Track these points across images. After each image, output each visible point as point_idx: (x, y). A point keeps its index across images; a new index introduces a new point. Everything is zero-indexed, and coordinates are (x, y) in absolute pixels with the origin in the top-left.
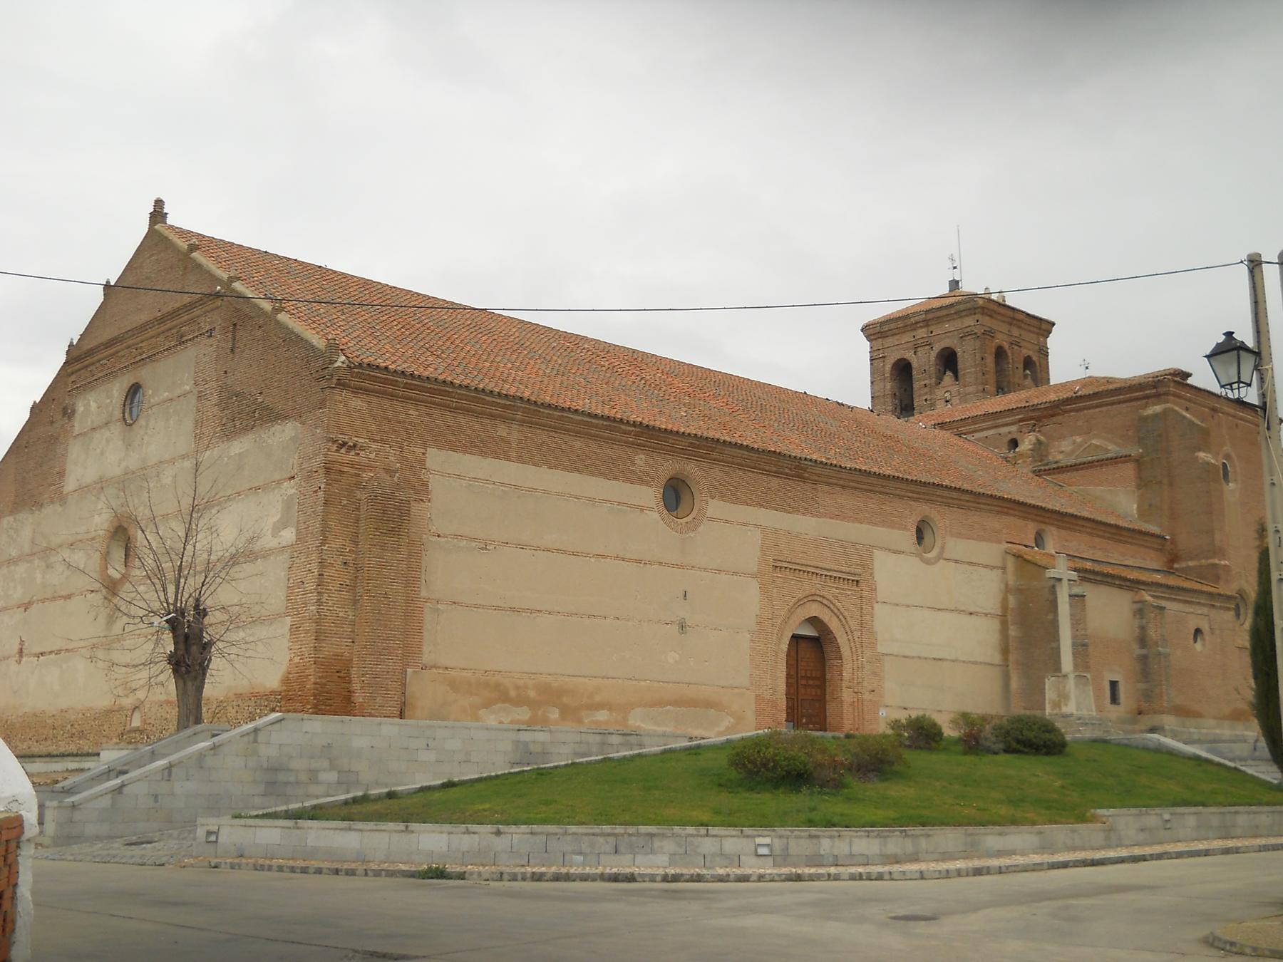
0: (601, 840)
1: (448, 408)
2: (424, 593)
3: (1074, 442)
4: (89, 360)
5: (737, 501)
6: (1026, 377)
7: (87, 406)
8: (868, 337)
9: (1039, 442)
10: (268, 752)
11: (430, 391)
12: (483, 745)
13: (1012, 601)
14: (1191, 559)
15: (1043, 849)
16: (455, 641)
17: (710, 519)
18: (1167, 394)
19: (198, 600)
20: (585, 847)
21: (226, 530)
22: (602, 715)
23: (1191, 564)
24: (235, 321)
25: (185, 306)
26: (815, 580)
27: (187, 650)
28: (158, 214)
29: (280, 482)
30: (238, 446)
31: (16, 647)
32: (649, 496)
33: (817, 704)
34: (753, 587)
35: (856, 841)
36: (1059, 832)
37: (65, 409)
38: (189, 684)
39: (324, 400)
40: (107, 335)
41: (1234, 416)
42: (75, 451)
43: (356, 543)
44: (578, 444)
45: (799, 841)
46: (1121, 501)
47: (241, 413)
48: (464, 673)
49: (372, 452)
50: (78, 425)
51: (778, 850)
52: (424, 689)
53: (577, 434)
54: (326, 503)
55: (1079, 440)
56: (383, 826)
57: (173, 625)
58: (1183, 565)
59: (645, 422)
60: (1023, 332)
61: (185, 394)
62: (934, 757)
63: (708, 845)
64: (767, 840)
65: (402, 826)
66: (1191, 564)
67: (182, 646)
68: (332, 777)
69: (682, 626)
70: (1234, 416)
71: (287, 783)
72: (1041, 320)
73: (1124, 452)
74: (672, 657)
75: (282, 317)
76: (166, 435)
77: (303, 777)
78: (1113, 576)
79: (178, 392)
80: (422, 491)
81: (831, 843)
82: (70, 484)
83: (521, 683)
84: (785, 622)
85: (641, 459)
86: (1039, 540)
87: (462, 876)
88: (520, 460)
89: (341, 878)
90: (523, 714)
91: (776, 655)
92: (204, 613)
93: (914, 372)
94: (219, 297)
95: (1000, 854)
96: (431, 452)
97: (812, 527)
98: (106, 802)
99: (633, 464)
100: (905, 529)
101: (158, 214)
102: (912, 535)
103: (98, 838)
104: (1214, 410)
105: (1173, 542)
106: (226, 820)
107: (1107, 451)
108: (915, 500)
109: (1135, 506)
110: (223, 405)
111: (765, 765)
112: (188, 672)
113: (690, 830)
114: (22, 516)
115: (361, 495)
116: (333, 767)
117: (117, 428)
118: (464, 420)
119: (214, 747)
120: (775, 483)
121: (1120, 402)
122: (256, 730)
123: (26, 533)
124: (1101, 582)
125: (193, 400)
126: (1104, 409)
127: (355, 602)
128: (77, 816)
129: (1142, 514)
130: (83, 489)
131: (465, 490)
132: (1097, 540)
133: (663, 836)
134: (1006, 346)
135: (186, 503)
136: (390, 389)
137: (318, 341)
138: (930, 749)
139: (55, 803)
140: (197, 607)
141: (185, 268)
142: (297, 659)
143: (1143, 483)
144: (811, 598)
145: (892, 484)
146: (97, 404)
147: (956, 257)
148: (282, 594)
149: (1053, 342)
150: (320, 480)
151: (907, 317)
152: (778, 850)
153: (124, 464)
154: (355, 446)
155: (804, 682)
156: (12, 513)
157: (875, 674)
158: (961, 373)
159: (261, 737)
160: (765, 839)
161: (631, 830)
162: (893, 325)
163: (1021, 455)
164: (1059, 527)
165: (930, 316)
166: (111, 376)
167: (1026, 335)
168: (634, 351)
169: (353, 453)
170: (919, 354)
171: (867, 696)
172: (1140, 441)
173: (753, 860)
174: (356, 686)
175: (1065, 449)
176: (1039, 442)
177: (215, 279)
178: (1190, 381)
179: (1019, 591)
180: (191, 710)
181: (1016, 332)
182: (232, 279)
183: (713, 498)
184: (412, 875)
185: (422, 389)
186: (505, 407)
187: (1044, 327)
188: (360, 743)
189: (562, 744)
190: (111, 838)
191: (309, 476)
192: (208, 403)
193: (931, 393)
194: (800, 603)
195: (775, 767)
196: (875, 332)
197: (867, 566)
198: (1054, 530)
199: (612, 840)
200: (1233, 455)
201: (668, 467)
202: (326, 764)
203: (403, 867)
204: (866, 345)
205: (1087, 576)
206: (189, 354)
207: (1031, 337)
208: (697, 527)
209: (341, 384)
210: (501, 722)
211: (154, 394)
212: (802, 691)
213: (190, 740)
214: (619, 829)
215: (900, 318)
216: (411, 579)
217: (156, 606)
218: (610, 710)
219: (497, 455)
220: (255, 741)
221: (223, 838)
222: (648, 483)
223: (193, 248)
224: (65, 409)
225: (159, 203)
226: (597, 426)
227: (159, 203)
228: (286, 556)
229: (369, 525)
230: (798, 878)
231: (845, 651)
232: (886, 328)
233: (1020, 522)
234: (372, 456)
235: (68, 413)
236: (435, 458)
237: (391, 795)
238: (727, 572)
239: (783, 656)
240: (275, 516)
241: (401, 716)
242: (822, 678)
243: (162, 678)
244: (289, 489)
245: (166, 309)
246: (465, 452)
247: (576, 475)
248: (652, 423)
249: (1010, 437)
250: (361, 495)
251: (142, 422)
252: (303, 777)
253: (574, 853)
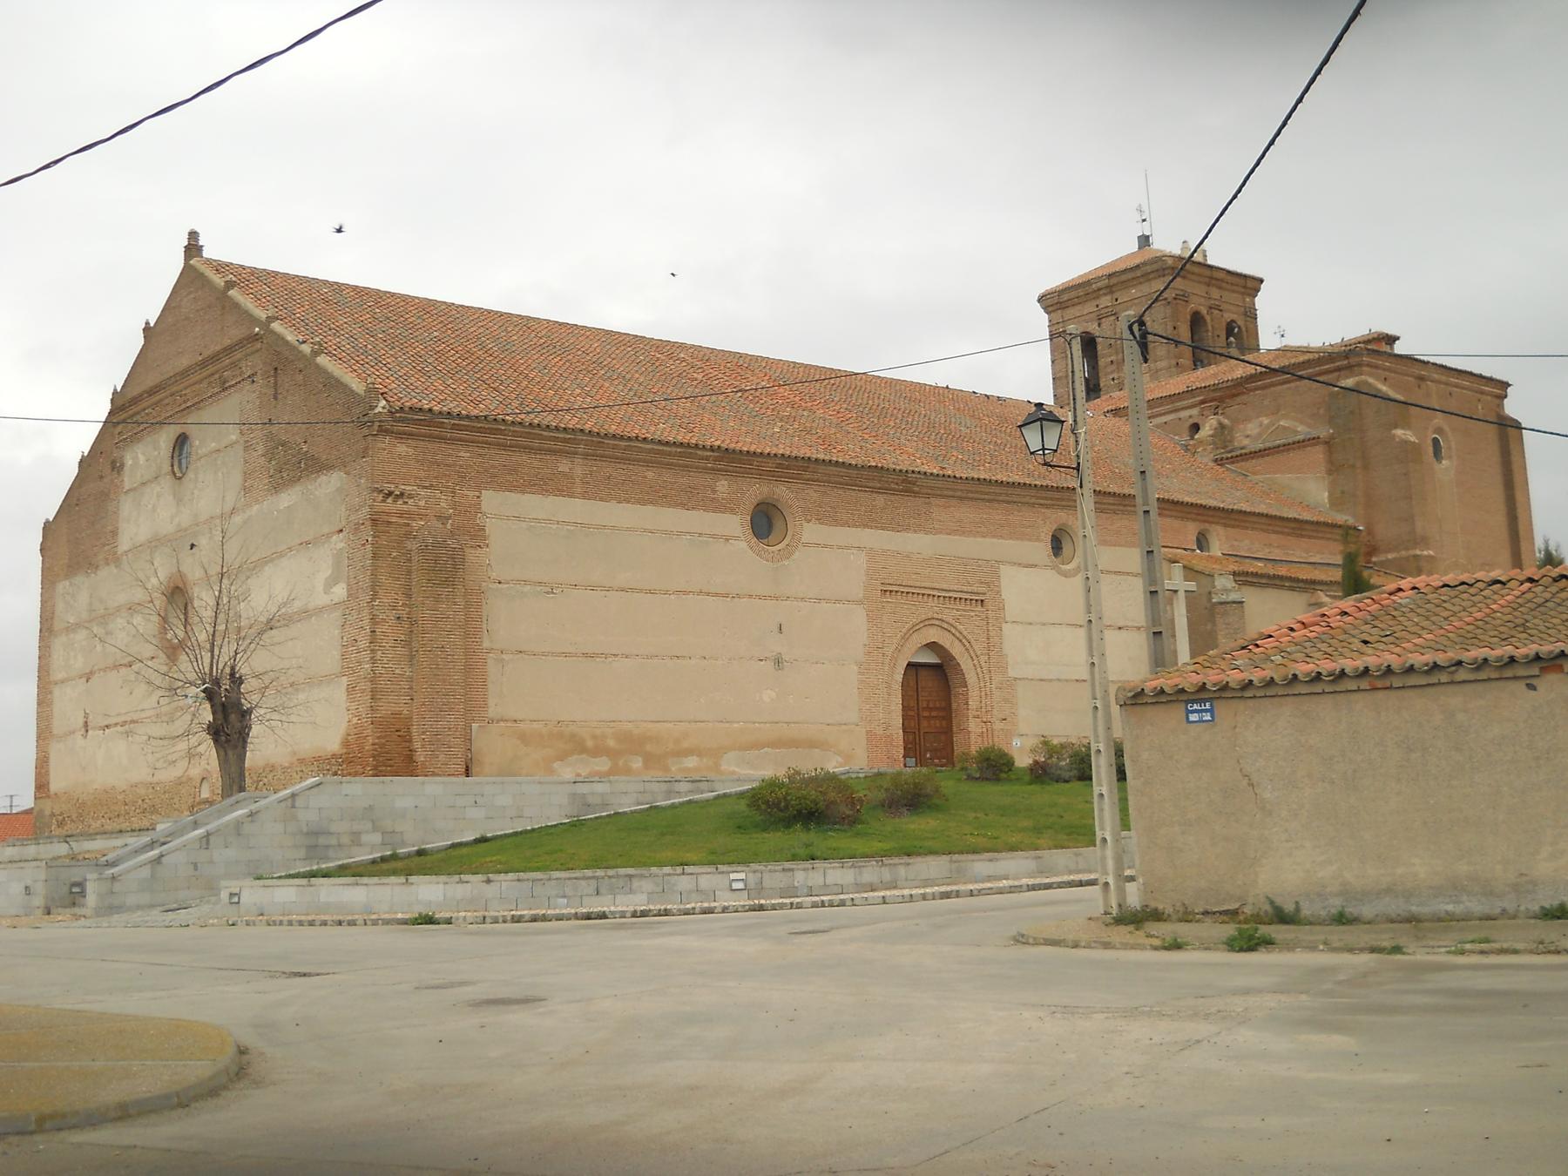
0: (583, 883)
1: (503, 446)
2: (486, 644)
4: (135, 409)
5: (837, 522)
6: (1229, 345)
7: (135, 459)
8: (1046, 309)
9: (1222, 426)
10: (308, 816)
11: (480, 430)
12: (540, 800)
14: (1389, 551)
15: (1041, 872)
16: (518, 694)
17: (806, 545)
18: (1359, 365)
19: (233, 668)
20: (569, 891)
21: (264, 594)
22: (691, 762)
23: (1390, 556)
25: (225, 349)
26: (931, 602)
27: (226, 717)
28: (193, 248)
29: (329, 536)
30: (287, 499)
31: (81, 721)
32: (735, 524)
33: (943, 737)
34: (859, 617)
35: (829, 872)
36: (1061, 858)
37: (113, 462)
38: (230, 753)
39: (366, 448)
40: (151, 380)
41: (1446, 384)
42: (126, 507)
43: (409, 596)
44: (650, 474)
45: (773, 876)
46: (1309, 490)
47: (290, 464)
48: (535, 725)
49: (422, 499)
51: (752, 884)
52: (491, 744)
53: (648, 464)
54: (375, 557)
55: (1266, 421)
56: (385, 880)
57: (210, 695)
58: (1382, 558)
59: (724, 446)
60: (1226, 294)
61: (231, 445)
62: (1005, 787)
63: (684, 883)
64: (742, 876)
65: (402, 879)
66: (1390, 556)
67: (220, 716)
68: (376, 838)
69: (778, 662)
70: (1446, 384)
71: (327, 847)
72: (1245, 277)
73: (1314, 434)
74: (768, 695)
75: (322, 360)
76: (216, 484)
77: (345, 840)
78: (1281, 578)
79: (225, 442)
80: (478, 536)
81: (805, 876)
82: (124, 544)
83: (598, 732)
84: (898, 650)
85: (723, 486)
86: (1202, 542)
87: (449, 922)
88: (585, 496)
89: (345, 929)
90: (603, 764)
91: (889, 687)
92: (240, 681)
93: (1099, 348)
94: (257, 339)
95: (989, 878)
96: (487, 495)
97: (928, 546)
98: (145, 872)
99: (714, 492)
100: (1038, 540)
101: (193, 248)
102: (1045, 548)
103: (139, 907)
104: (1422, 378)
105: (1370, 532)
106: (249, 882)
107: (1296, 432)
108: (1047, 506)
110: (270, 455)
111: (777, 805)
112: (228, 741)
113: (667, 870)
114: (79, 579)
115: (412, 545)
116: (375, 829)
117: (167, 482)
119: (251, 814)
120: (880, 500)
122: (293, 795)
123: (83, 599)
124: (1267, 586)
125: (239, 448)
127: (412, 657)
128: (117, 887)
129: (1336, 502)
130: (136, 548)
131: (527, 533)
132: (1273, 536)
133: (642, 876)
134: (1204, 311)
135: (214, 570)
136: (435, 431)
137: (358, 386)
138: (998, 780)
139: (95, 876)
140: (232, 675)
142: (355, 720)
143: (1334, 468)
144: (928, 623)
145: (1018, 491)
146: (146, 456)
147: (1145, 208)
148: (336, 654)
149: (1260, 301)
150: (367, 533)
151: (1088, 283)
152: (752, 884)
153: (176, 520)
154: (402, 494)
155: (926, 714)
156: (67, 577)
157: (1006, 701)
159: (299, 802)
160: (738, 876)
161: (611, 872)
162: (1073, 294)
163: (1201, 442)
164: (1225, 525)
165: (1114, 281)
167: (1227, 296)
168: (741, 355)
171: (998, 726)
172: (1331, 421)
173: (729, 894)
174: (417, 745)
175: (1251, 432)
176: (1222, 426)
177: (254, 321)
178: (1399, 348)
180: (235, 780)
181: (1215, 293)
182: (271, 319)
184: (405, 922)
185: (472, 429)
186: (565, 441)
187: (1250, 285)
188: (400, 803)
189: (627, 794)
190: (152, 906)
191: (357, 528)
193: (1119, 369)
194: (915, 629)
195: (787, 807)
196: (1054, 302)
197: (993, 583)
198: (1220, 529)
199: (593, 882)
200: (1446, 428)
201: (756, 491)
202: (369, 826)
203: (400, 916)
204: (1044, 318)
205: (1245, 579)
207: (1233, 298)
208: (791, 554)
209: (383, 431)
210: (578, 775)
211: (201, 443)
212: (924, 723)
213: (233, 807)
214: (600, 873)
215: (1080, 286)
216: (471, 626)
217: (192, 676)
218: (700, 755)
219: (560, 492)
220: (293, 807)
221: (246, 897)
222: (732, 511)
223: (230, 285)
224: (113, 462)
225: (193, 235)
226: (670, 454)
227: (193, 235)
228: (337, 614)
229: (421, 579)
230: (761, 908)
231: (971, 678)
232: (1065, 297)
233: (1177, 523)
234: (422, 503)
235: (117, 467)
236: (492, 500)
237: (420, 853)
238: (828, 601)
239: (897, 687)
240: (326, 572)
241: (467, 773)
242: (948, 709)
243: (201, 749)
244: (338, 542)
245: (207, 353)
246: (523, 492)
247: (650, 507)
248: (732, 446)
249: (1191, 421)
250: (412, 545)
251: (191, 475)
252: (345, 840)
253: (558, 896)
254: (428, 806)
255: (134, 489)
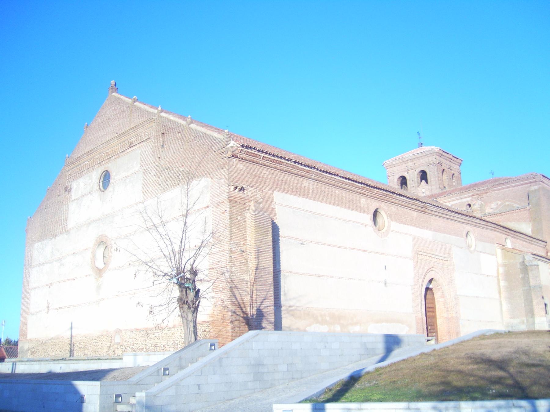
3: (497, 204)
13: (501, 270)
24: (163, 131)
50: (74, 195)
55: (499, 203)
82: (71, 224)
85: (363, 200)
88: (314, 199)
99: (360, 203)
109: (530, 230)
118: (289, 177)
121: (518, 185)
126: (511, 189)
136: (256, 159)
141: (132, 110)
145: (458, 216)
150: (227, 206)
156: (39, 241)
158: (429, 181)
164: (513, 237)
166: (90, 168)
169: (241, 192)
170: (410, 173)
176: (482, 205)
179: (505, 265)
183: (392, 220)
192: (149, 175)
201: (374, 204)
206: (137, 152)
217: (167, 270)
222: (366, 212)
234: (250, 194)
236: (278, 197)
249: (467, 203)
254: (72, 358)
255: (78, 199)
